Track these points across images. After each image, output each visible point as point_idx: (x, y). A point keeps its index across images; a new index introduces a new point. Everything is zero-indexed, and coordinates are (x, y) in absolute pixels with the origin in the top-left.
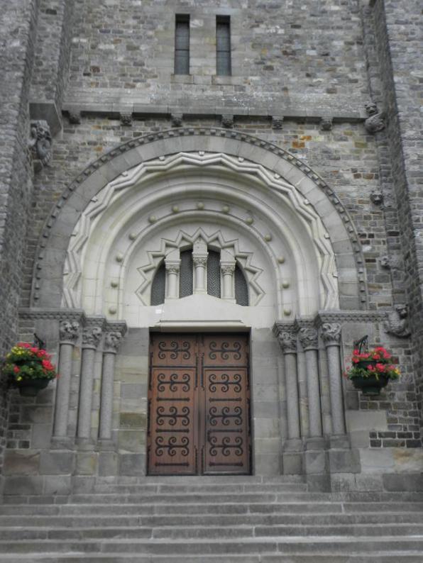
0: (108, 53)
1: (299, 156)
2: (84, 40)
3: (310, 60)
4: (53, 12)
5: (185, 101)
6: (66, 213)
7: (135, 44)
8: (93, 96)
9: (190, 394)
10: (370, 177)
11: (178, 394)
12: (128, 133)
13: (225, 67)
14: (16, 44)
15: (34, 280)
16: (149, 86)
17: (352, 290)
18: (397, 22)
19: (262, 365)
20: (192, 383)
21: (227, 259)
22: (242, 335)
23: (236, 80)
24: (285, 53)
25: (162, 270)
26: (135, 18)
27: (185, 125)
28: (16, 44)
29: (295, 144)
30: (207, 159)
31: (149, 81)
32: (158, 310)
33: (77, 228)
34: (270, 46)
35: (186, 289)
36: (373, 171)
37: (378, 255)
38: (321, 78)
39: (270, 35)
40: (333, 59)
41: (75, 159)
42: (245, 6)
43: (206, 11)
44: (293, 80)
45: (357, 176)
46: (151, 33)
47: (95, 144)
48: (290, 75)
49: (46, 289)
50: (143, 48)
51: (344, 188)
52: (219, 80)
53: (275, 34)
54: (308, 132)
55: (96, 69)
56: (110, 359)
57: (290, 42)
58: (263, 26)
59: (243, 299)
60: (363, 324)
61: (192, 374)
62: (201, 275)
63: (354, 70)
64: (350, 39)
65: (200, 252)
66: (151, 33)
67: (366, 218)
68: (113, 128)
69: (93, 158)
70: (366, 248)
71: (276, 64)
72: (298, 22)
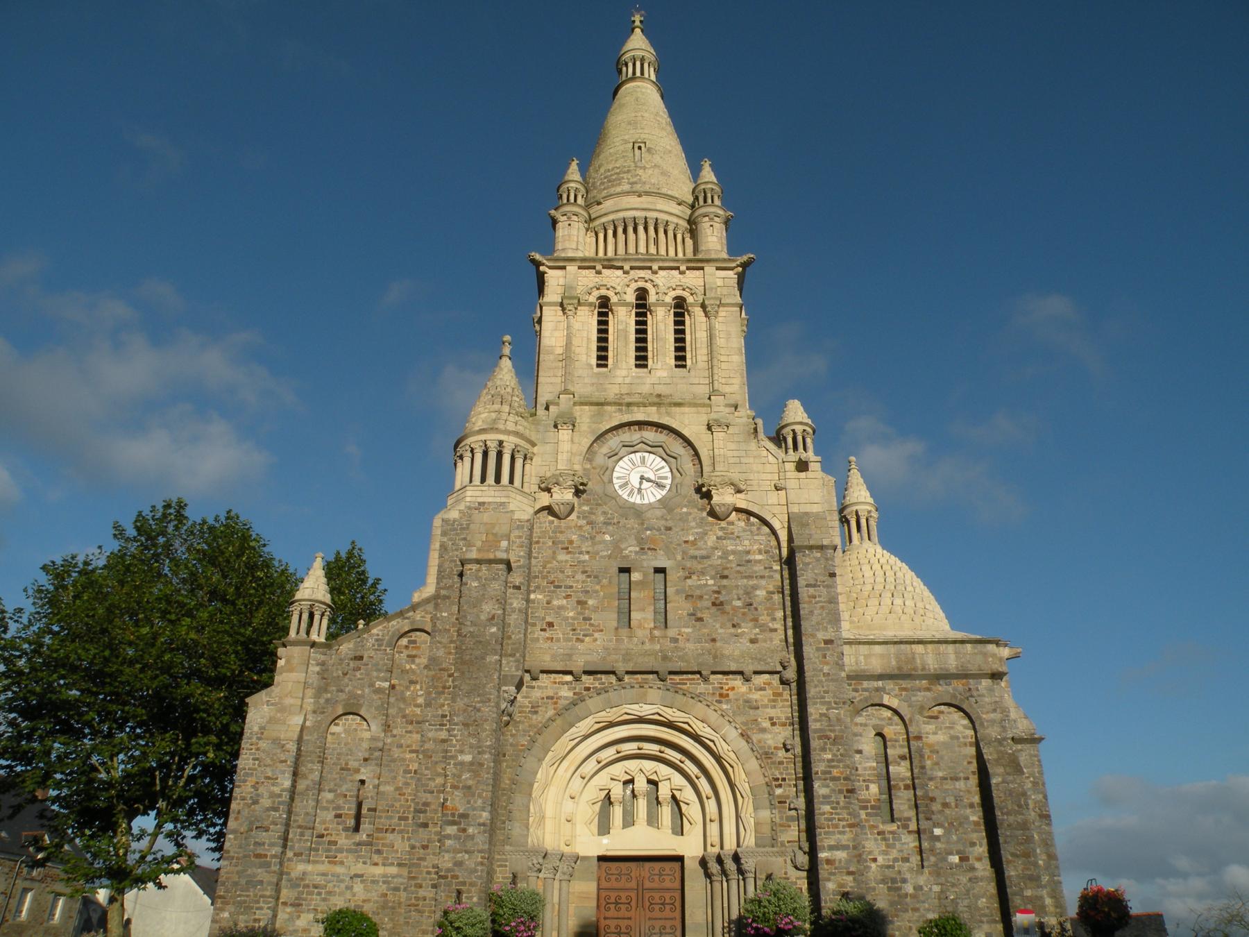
0: (561, 608)
1: (725, 707)
2: (540, 597)
3: (735, 609)
4: (518, 588)
5: (627, 657)
6: (529, 762)
7: (583, 599)
8: (544, 652)
9: (632, 914)
10: (784, 725)
11: (620, 914)
12: (579, 687)
13: (664, 621)
14: (494, 630)
15: (449, 661)
16: (596, 640)
17: (766, 830)
18: (807, 586)
19: (696, 886)
20: (633, 903)
21: (664, 791)
22: (680, 859)
23: (672, 632)
24: (714, 604)
25: (608, 800)
26: (584, 572)
27: (626, 678)
28: (494, 630)
29: (721, 695)
30: (645, 710)
31: (597, 635)
32: (605, 840)
33: (539, 776)
34: (701, 597)
35: (629, 821)
36: (787, 718)
37: (788, 797)
38: (746, 629)
39: (700, 587)
40: (756, 609)
41: (536, 712)
42: (679, 557)
43: (645, 564)
44: (720, 631)
45: (773, 724)
46: (598, 587)
47: (552, 698)
48: (718, 626)
49: (516, 830)
50: (590, 602)
51: (761, 736)
52: (656, 633)
53: (706, 585)
54: (732, 683)
55: (551, 625)
56: (564, 884)
57: (718, 592)
58: (694, 577)
59: (679, 830)
60: (774, 859)
61: (633, 894)
62: (642, 805)
63: (774, 619)
64: (771, 588)
65: (641, 784)
66: (598, 587)
67: (781, 763)
68: (567, 683)
69: (551, 713)
70: (779, 791)
71: (705, 615)
72: (726, 572)
